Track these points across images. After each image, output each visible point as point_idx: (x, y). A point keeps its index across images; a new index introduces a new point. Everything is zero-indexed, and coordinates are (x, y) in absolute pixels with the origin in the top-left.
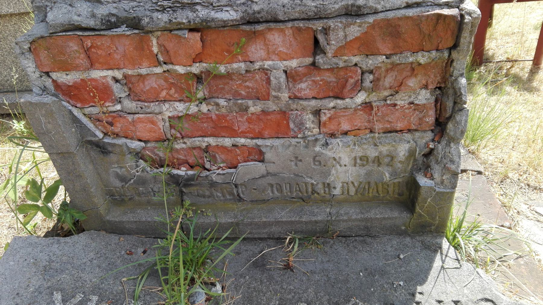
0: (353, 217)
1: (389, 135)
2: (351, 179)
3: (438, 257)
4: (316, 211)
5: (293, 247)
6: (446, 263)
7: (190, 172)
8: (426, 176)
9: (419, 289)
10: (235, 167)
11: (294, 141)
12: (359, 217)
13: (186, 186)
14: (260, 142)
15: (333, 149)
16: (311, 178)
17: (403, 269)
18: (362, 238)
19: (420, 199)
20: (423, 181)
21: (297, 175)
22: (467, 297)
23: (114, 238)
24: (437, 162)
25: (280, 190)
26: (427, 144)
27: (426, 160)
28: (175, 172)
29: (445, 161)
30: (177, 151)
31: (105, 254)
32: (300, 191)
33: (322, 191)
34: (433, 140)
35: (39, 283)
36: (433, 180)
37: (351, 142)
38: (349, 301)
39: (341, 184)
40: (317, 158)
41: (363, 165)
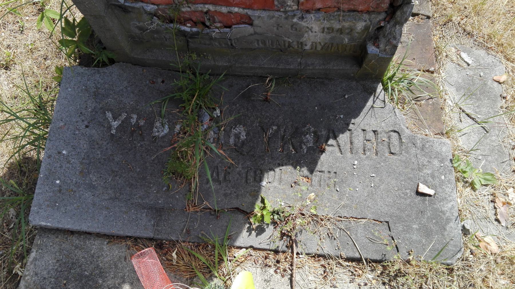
0: (317, 68)
1: (352, 14)
2: (319, 41)
3: (372, 98)
4: (290, 60)
5: (271, 86)
6: (376, 103)
7: (195, 29)
8: (374, 45)
9: (353, 121)
10: (230, 27)
11: (277, 14)
12: (321, 68)
13: (190, 38)
14: (250, 12)
15: (307, 21)
16: (288, 38)
17: (345, 106)
18: (321, 80)
19: (367, 60)
20: (371, 49)
21: (278, 36)
22: (383, 128)
23: (139, 69)
24: (384, 36)
25: (264, 43)
26: (379, 22)
27: (376, 34)
28: (183, 28)
29: (390, 37)
30: (183, 12)
31: (135, 83)
32: (279, 45)
33: (296, 46)
34: (384, 20)
35: (94, 105)
36: (378, 48)
37: (321, 18)
38: (306, 126)
39: (311, 43)
40: (294, 26)
41: (329, 33)
